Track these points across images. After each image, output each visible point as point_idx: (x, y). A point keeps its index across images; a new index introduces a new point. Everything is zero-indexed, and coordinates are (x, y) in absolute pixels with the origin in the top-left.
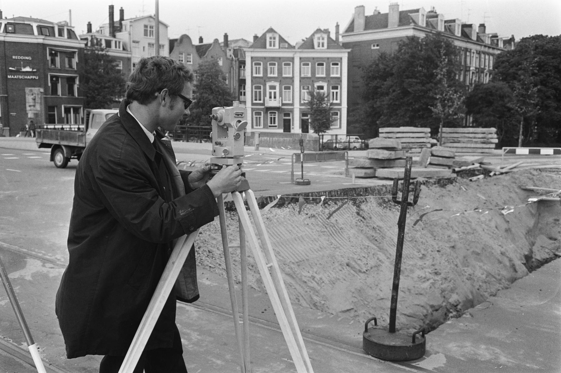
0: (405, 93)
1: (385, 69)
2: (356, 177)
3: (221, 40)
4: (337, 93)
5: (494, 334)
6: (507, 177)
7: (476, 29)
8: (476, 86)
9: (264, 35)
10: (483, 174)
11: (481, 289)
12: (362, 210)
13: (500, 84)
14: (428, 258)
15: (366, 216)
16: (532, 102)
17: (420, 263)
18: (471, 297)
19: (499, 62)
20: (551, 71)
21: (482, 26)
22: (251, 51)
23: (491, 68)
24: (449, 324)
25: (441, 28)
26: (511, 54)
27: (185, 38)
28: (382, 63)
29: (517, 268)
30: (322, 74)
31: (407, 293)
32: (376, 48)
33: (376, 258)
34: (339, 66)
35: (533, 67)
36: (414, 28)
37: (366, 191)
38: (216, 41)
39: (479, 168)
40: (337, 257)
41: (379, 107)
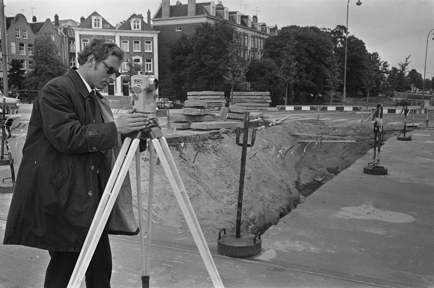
0: (203, 65)
1: (186, 47)
2: (177, 129)
3: (53, 20)
4: (150, 65)
5: (302, 233)
6: (281, 127)
7: (251, 19)
8: (252, 61)
9: (90, 17)
10: (264, 125)
11: (269, 207)
12: (183, 154)
13: (269, 60)
14: (232, 187)
15: (186, 159)
16: (293, 73)
17: (227, 191)
18: (263, 213)
19: (268, 43)
20: (302, 51)
21: (255, 17)
22: (80, 30)
23: (262, 48)
24: (271, 229)
25: (226, 17)
26: (275, 39)
27: (20, 17)
28: (184, 43)
29: (292, 191)
30: (138, 50)
31: (220, 213)
32: (179, 30)
33: (196, 189)
34: (151, 44)
35: (293, 48)
36: (207, 17)
37: (185, 139)
38: (48, 20)
39: (261, 121)
40: (168, 190)
41: (183, 76)
